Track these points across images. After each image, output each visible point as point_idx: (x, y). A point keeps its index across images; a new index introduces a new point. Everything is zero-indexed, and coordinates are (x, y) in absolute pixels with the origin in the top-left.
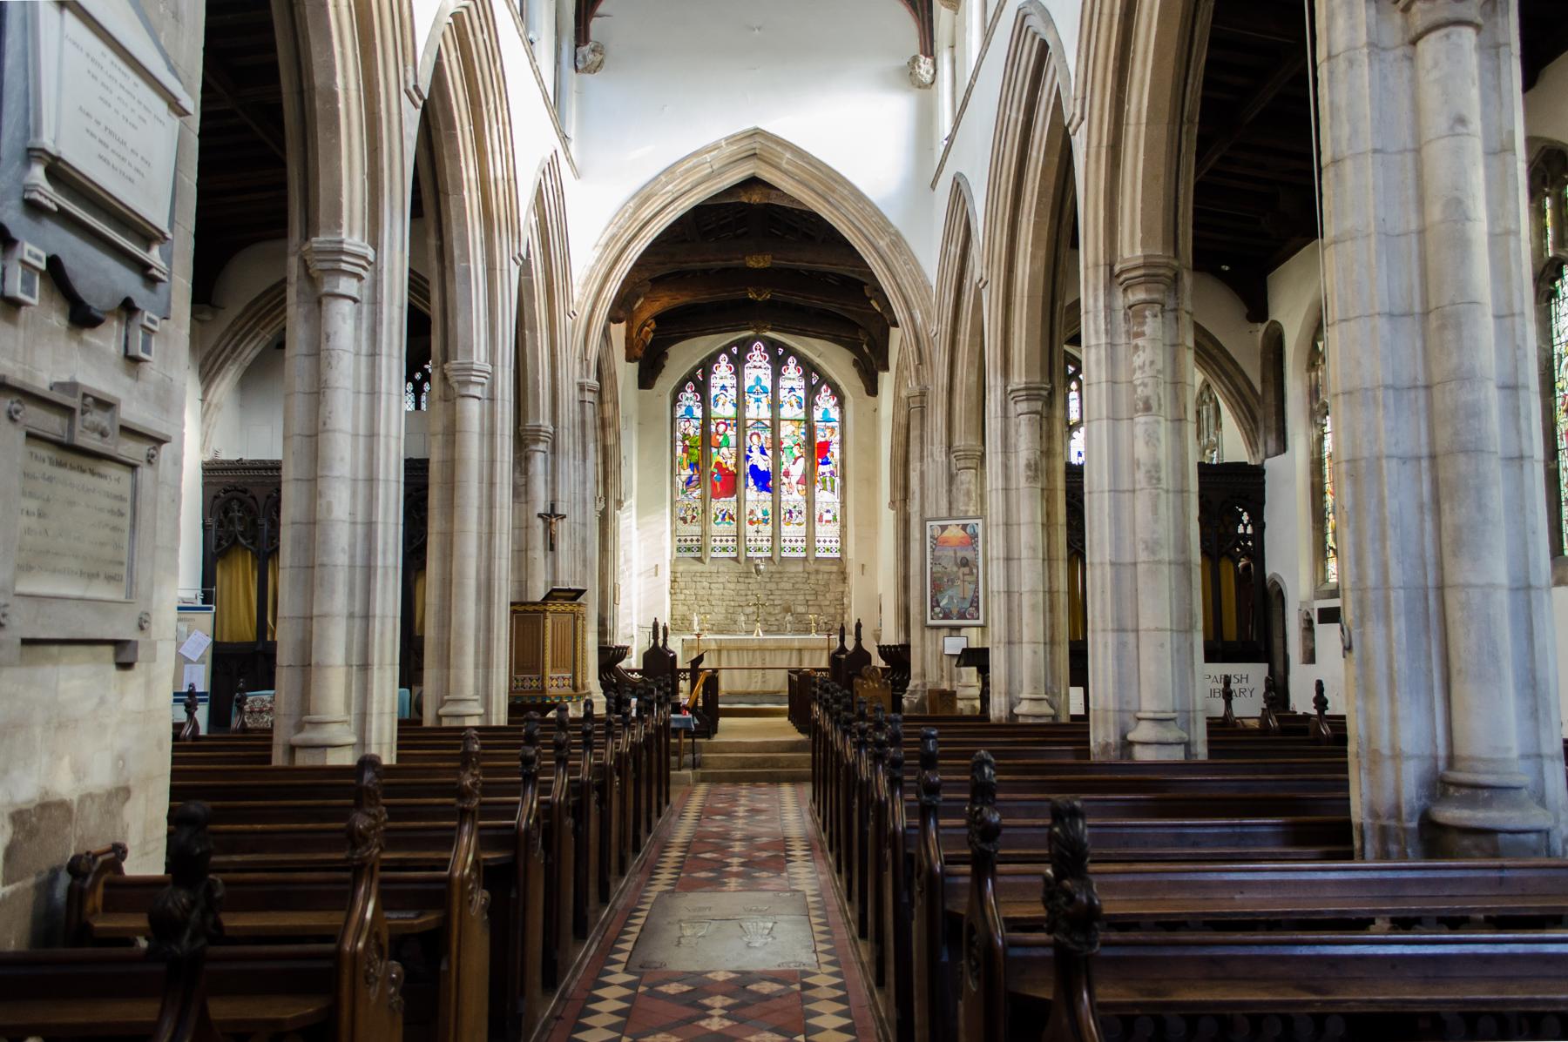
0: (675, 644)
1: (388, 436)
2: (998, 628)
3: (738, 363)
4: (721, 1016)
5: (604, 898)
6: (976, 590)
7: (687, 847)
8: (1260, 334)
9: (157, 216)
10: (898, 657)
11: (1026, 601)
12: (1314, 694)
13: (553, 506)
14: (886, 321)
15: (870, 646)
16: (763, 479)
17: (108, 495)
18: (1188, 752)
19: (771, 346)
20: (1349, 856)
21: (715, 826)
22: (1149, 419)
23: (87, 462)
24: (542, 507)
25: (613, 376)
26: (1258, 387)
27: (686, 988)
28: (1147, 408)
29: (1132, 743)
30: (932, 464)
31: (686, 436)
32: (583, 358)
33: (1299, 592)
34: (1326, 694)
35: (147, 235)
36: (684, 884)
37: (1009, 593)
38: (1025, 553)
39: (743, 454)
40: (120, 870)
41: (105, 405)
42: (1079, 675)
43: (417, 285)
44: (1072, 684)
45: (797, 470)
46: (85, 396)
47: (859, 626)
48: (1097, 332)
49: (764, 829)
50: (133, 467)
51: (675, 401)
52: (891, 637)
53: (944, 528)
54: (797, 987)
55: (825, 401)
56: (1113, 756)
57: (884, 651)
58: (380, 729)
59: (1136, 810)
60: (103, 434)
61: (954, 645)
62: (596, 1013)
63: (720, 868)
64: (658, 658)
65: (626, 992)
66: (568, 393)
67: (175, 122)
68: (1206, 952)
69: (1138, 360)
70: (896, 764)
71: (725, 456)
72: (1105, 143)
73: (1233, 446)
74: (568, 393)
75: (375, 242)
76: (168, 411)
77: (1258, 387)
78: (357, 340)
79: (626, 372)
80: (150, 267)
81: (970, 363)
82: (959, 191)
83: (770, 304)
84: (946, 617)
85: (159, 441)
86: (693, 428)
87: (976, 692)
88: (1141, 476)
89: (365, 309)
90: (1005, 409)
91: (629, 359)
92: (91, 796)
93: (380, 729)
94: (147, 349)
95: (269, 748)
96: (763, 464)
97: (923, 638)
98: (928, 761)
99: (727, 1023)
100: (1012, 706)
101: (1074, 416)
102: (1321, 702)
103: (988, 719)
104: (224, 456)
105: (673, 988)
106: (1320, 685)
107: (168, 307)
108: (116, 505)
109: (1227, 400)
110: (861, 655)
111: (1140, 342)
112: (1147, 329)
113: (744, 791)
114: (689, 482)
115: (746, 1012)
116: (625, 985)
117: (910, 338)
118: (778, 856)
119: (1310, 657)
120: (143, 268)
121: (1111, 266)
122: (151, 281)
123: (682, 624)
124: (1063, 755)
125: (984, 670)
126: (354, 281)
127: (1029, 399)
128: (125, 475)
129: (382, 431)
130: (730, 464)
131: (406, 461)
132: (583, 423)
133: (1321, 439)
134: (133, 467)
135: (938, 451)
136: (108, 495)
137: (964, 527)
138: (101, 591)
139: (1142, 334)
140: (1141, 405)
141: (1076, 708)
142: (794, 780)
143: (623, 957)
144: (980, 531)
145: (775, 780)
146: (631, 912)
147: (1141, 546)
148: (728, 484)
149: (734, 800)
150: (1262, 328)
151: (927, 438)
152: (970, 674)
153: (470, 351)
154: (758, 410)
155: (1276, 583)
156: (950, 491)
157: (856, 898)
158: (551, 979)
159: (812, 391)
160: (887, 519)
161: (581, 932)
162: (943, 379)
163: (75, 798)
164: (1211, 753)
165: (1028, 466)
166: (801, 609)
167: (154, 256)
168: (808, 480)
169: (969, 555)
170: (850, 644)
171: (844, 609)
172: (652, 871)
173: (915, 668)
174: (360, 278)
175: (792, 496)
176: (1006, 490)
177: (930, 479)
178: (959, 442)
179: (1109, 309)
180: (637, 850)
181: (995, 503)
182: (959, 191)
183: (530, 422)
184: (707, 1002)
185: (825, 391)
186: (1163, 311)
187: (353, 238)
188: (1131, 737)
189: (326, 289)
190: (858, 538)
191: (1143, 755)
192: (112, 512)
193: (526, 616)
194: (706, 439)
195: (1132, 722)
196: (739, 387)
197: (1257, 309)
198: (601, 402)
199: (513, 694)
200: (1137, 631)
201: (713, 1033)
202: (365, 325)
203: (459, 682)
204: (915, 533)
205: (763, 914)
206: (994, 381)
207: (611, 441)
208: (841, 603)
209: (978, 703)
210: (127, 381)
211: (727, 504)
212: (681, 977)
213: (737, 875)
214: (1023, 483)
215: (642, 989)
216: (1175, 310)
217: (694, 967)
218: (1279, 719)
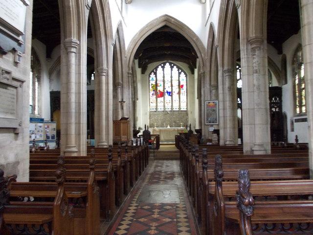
0: (151, 130)
1: (83, 83)
2: (221, 125)
3: (163, 67)
4: (158, 214)
5: (132, 185)
6: (216, 117)
7: (152, 174)
8: (281, 58)
9: (21, 28)
10: (199, 131)
11: (228, 118)
12: (295, 138)
13: (122, 99)
14: (196, 57)
15: (193, 129)
16: (170, 94)
17: (10, 94)
18: (266, 152)
19: (170, 64)
20: (308, 178)
21: (159, 169)
22: (257, 75)
23: (4, 86)
24: (120, 100)
25: (136, 71)
26: (280, 69)
27: (149, 207)
28: (256, 72)
29: (253, 150)
30: (206, 88)
31: (152, 84)
32: (129, 67)
33: (290, 116)
34: (298, 138)
35: (19, 33)
36: (151, 182)
37: (224, 117)
38: (228, 108)
39: (164, 88)
40: (15, 181)
41: (8, 73)
42: (240, 134)
43: (90, 50)
44: (239, 138)
45: (177, 90)
46: (3, 70)
47: (190, 125)
48: (244, 55)
49: (170, 170)
50: (16, 88)
51: (150, 76)
52: (197, 128)
53: (209, 103)
54: (175, 207)
55: (183, 75)
56: (249, 154)
57: (197, 131)
58: (83, 148)
59: (255, 167)
60: (8, 79)
61: (212, 129)
62: (128, 213)
63: (159, 179)
64: (146, 134)
65: (135, 208)
66: (125, 75)
67: (24, 7)
68: (278, 206)
69: (255, 61)
70: (197, 157)
71: (160, 89)
72: (245, 10)
73: (275, 83)
74: (125, 75)
75: (79, 40)
76: (26, 75)
77: (280, 69)
78: (76, 62)
79: (139, 71)
80: (19, 41)
81: (215, 65)
82: (211, 27)
83: (170, 54)
84: (210, 123)
85: (23, 82)
86: (153, 83)
87: (217, 139)
88: (255, 88)
89: (77, 54)
90: (223, 75)
91: (139, 67)
92: (9, 163)
93: (83, 148)
94: (19, 60)
95: (60, 152)
96: (170, 90)
97: (205, 127)
98: (205, 156)
99: (158, 216)
100: (225, 142)
101: (238, 77)
102: (297, 140)
103: (219, 145)
104: (54, 90)
105: (146, 207)
106: (297, 136)
107: (25, 50)
108: (13, 96)
109: (273, 72)
110: (191, 131)
111: (255, 56)
112: (256, 53)
113: (165, 161)
114: (153, 94)
115: (162, 213)
116: (136, 206)
117: (201, 60)
118: (171, 176)
119: (293, 130)
120: (17, 41)
121: (247, 39)
122: (20, 44)
123: (152, 126)
124: (237, 153)
125: (218, 134)
126: (75, 49)
127: (228, 72)
128: (15, 90)
129: (82, 82)
130: (162, 90)
131: (87, 91)
132: (129, 81)
133: (295, 81)
134: (16, 88)
135: (208, 86)
136: (10, 94)
137: (214, 102)
138: (9, 116)
139: (255, 55)
140: (255, 71)
141: (240, 142)
142: (176, 159)
143: (136, 199)
144: (217, 103)
145: (172, 159)
146: (138, 189)
147: (255, 105)
148: (162, 95)
149: (163, 164)
150: (281, 55)
151: (205, 82)
152: (215, 135)
153: (102, 66)
154: (168, 78)
155: (285, 114)
156: (210, 95)
157: (189, 186)
158: (118, 204)
159: (180, 73)
160: (197, 101)
161: (126, 193)
162: (209, 69)
163: (5, 164)
164: (272, 152)
165: (228, 88)
166: (178, 122)
167: (20, 38)
168: (179, 93)
169: (215, 109)
170: (188, 129)
171: (187, 121)
172: (144, 180)
173: (203, 134)
174: (76, 48)
175: (175, 96)
176: (223, 93)
177: (206, 92)
178: (212, 83)
179: (247, 49)
180: (140, 175)
181: (221, 96)
182: (211, 27)
183: (117, 81)
184: (154, 211)
185: (182, 73)
186: (260, 49)
187: (74, 39)
188: (253, 149)
189: (69, 50)
190: (190, 106)
191: (256, 153)
192: (11, 98)
193: (116, 123)
194: (156, 85)
195: (253, 146)
196: (164, 103)
197: (280, 51)
198: (133, 77)
199: (114, 140)
200: (254, 124)
201: (155, 218)
202: (77, 58)
203: (102, 138)
204: (203, 104)
205: (168, 190)
206: (220, 68)
207: (135, 85)
208: (187, 120)
209: (217, 142)
210: (15, 67)
211: (162, 99)
212: (149, 205)
213: (163, 181)
214: (227, 92)
215: (139, 207)
216: (263, 49)
217: (152, 202)
218: (287, 144)
